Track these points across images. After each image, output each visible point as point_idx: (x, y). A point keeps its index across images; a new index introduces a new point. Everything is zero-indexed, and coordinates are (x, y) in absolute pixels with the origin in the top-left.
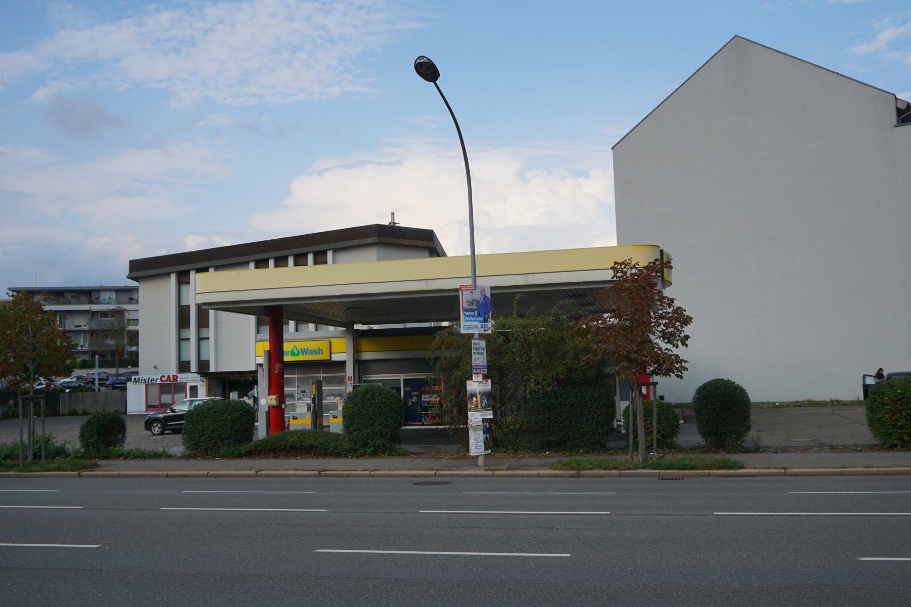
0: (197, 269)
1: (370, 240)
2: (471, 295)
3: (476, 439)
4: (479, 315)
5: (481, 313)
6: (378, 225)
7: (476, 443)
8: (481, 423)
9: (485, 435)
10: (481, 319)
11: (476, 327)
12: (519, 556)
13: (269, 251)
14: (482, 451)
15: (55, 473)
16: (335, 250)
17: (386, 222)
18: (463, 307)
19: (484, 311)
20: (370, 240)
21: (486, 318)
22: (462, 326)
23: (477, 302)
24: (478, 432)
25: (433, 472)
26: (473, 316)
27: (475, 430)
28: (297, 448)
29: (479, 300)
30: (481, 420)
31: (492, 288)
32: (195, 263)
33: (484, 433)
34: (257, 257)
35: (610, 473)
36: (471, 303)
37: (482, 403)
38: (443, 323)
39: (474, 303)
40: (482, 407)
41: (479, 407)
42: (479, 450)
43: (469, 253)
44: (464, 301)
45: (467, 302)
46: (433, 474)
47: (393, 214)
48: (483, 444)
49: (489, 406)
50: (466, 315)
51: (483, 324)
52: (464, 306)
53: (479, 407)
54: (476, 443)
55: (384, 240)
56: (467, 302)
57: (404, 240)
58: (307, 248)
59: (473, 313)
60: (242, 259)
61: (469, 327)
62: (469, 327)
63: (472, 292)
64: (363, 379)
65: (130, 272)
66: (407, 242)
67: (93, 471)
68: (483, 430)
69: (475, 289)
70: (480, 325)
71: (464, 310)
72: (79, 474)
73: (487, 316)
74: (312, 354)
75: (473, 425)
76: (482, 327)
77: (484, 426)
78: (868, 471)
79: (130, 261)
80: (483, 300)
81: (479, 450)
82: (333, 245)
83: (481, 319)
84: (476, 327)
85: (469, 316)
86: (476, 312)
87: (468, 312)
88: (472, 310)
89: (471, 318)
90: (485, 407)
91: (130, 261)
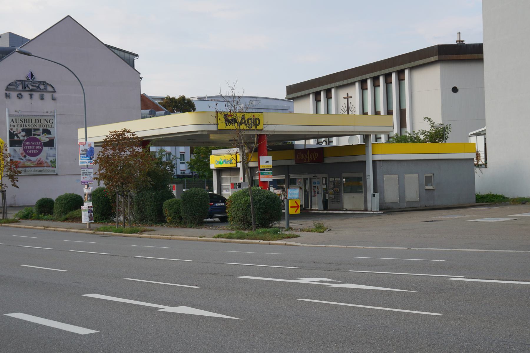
0: (326, 89)
1: (433, 59)
2: (84, 147)
3: (84, 215)
4: (87, 156)
5: (89, 155)
6: (438, 45)
7: (85, 217)
8: (87, 208)
9: (90, 214)
10: (89, 158)
11: (86, 162)
12: (44, 267)
13: (367, 73)
14: (87, 221)
15: (238, 240)
16: (411, 69)
17: (452, 41)
18: (80, 153)
19: (91, 154)
20: (433, 59)
21: (92, 158)
22: (80, 162)
23: (86, 150)
24: (86, 212)
25: (66, 230)
26: (84, 157)
27: (84, 211)
28: (77, 218)
29: (87, 149)
30: (87, 206)
31: (95, 143)
32: (323, 86)
33: (89, 213)
34: (359, 78)
35: (107, 234)
36: (83, 151)
37: (87, 199)
38: (296, 141)
39: (85, 151)
40: (88, 201)
41: (87, 200)
42: (86, 221)
43: (88, 128)
44: (80, 150)
45: (82, 150)
46: (137, 236)
47: (459, 33)
48: (88, 218)
49: (90, 200)
50: (81, 157)
51: (90, 161)
52: (81, 152)
53: (87, 200)
54: (85, 217)
55: (443, 57)
56: (82, 150)
57: (459, 55)
58: (391, 68)
59: (84, 156)
60: (350, 81)
61: (83, 163)
62: (83, 163)
63: (84, 146)
64: (253, 179)
65: (287, 94)
66: (468, 56)
67: (143, 234)
68: (88, 211)
69: (85, 144)
70: (87, 161)
71: (81, 154)
72: (1, 225)
73: (92, 157)
74: (228, 163)
75: (84, 209)
76: (89, 162)
77: (89, 209)
78: (154, 237)
79: (287, 87)
80: (90, 149)
81: (86, 221)
82: (407, 65)
83: (89, 158)
84: (86, 162)
85: (82, 157)
86: (86, 155)
87: (82, 155)
88: (83, 154)
89: (83, 158)
90: (89, 200)
91: (287, 87)
